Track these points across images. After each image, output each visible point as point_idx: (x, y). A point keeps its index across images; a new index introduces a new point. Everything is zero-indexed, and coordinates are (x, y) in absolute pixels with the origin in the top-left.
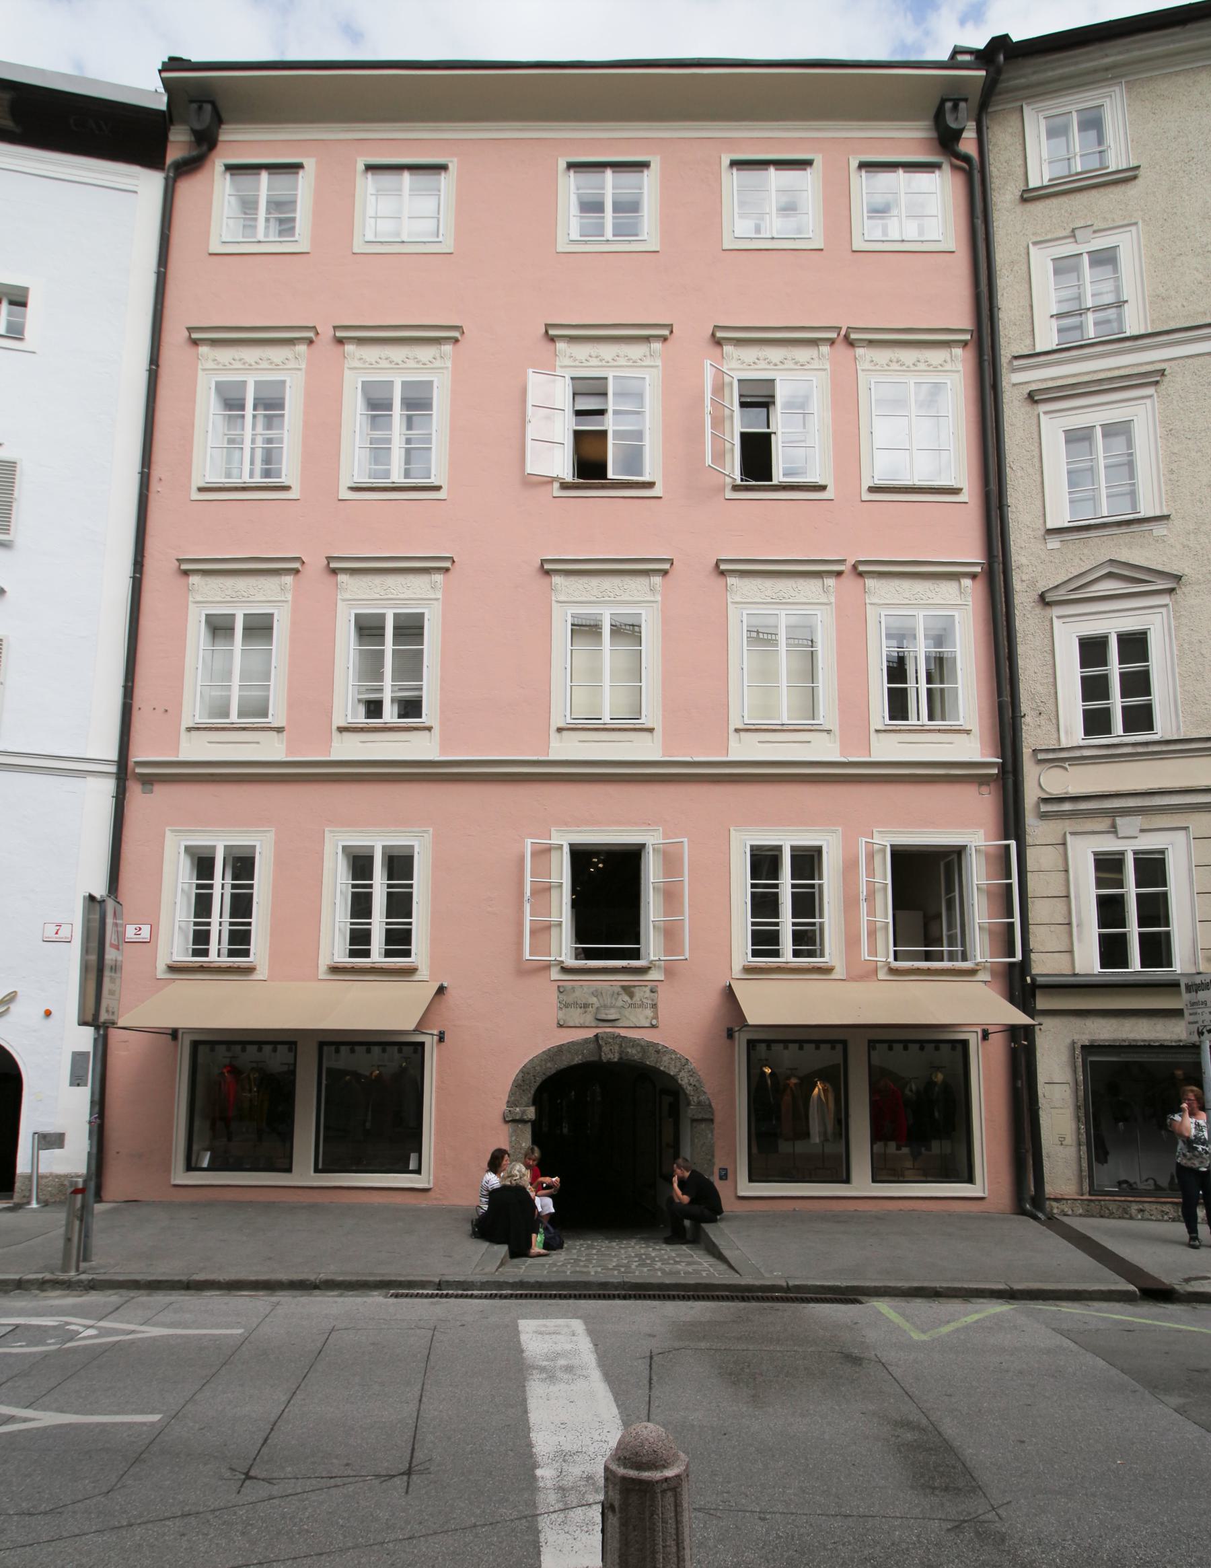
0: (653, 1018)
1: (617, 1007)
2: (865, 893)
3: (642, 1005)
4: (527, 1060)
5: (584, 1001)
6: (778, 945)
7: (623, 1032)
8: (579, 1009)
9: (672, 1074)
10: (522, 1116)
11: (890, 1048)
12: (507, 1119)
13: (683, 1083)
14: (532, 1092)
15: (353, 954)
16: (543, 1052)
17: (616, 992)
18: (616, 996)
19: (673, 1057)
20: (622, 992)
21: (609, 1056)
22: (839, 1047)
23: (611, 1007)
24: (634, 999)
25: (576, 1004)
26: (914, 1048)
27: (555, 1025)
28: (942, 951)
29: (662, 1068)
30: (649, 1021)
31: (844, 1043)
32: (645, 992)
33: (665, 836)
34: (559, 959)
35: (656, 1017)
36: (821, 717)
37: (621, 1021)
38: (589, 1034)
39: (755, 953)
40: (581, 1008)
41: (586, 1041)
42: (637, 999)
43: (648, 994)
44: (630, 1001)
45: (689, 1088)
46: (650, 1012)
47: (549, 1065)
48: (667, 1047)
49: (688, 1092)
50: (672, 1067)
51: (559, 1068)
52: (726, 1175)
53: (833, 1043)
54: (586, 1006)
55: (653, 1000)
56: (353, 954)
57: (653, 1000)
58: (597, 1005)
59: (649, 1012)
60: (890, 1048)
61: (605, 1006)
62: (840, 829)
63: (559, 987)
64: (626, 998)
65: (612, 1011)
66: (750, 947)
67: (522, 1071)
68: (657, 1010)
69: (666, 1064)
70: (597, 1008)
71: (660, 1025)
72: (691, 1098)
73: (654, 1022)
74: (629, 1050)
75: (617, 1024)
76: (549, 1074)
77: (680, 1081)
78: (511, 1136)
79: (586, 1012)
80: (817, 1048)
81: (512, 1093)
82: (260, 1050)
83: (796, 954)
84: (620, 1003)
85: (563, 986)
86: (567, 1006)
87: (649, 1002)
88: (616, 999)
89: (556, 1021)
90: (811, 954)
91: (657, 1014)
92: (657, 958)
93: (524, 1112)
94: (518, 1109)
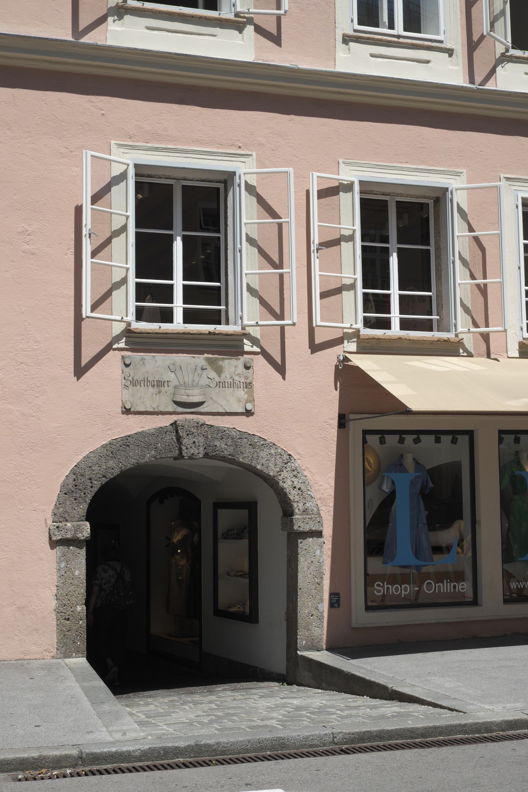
0: (247, 401)
1: (202, 387)
2: (89, 226)
3: (233, 385)
4: (81, 457)
5: (157, 378)
6: (172, 303)
7: (209, 420)
8: (150, 387)
9: (271, 474)
10: (75, 533)
11: (438, 440)
12: (54, 538)
13: (285, 486)
14: (88, 501)
15: (368, 323)
16: (103, 446)
17: (199, 366)
18: (199, 371)
19: (273, 451)
20: (208, 367)
21: (192, 451)
22: (464, 440)
23: (193, 386)
24: (223, 376)
25: (146, 382)
26: (446, 439)
27: (120, 410)
28: (431, 320)
29: (259, 467)
30: (242, 405)
31: (470, 434)
32: (236, 367)
33: (260, 164)
34: (354, 326)
35: (251, 400)
36: (442, 32)
37: (205, 404)
38: (165, 421)
39: (140, 314)
40: (153, 386)
41: (161, 431)
42: (226, 376)
43: (241, 369)
44: (217, 379)
45: (293, 492)
46: (243, 393)
47: (111, 463)
48: (265, 440)
49: (291, 497)
50: (272, 466)
51: (123, 468)
52: (338, 601)
53: (454, 434)
54: (160, 384)
55: (246, 378)
56: (368, 323)
57: (246, 378)
58: (174, 382)
59: (241, 393)
60: (438, 440)
61: (186, 386)
62: (464, 171)
63: (123, 357)
64: (213, 374)
65: (196, 391)
66: (361, 315)
67: (73, 472)
68: (253, 392)
69: (264, 461)
70: (175, 387)
71: (256, 411)
72: (295, 505)
73: (249, 407)
74: (217, 443)
75: (201, 409)
76: (110, 476)
77: (281, 483)
78: (59, 563)
79: (160, 392)
80: (438, 440)
81: (59, 503)
82: (401, 441)
83: (405, 325)
84: (204, 381)
85: (129, 357)
86: (135, 383)
87: (243, 380)
88: (200, 376)
89: (120, 404)
90: (427, 326)
91: (253, 396)
92: (253, 323)
93: (77, 529)
94: (69, 524)
